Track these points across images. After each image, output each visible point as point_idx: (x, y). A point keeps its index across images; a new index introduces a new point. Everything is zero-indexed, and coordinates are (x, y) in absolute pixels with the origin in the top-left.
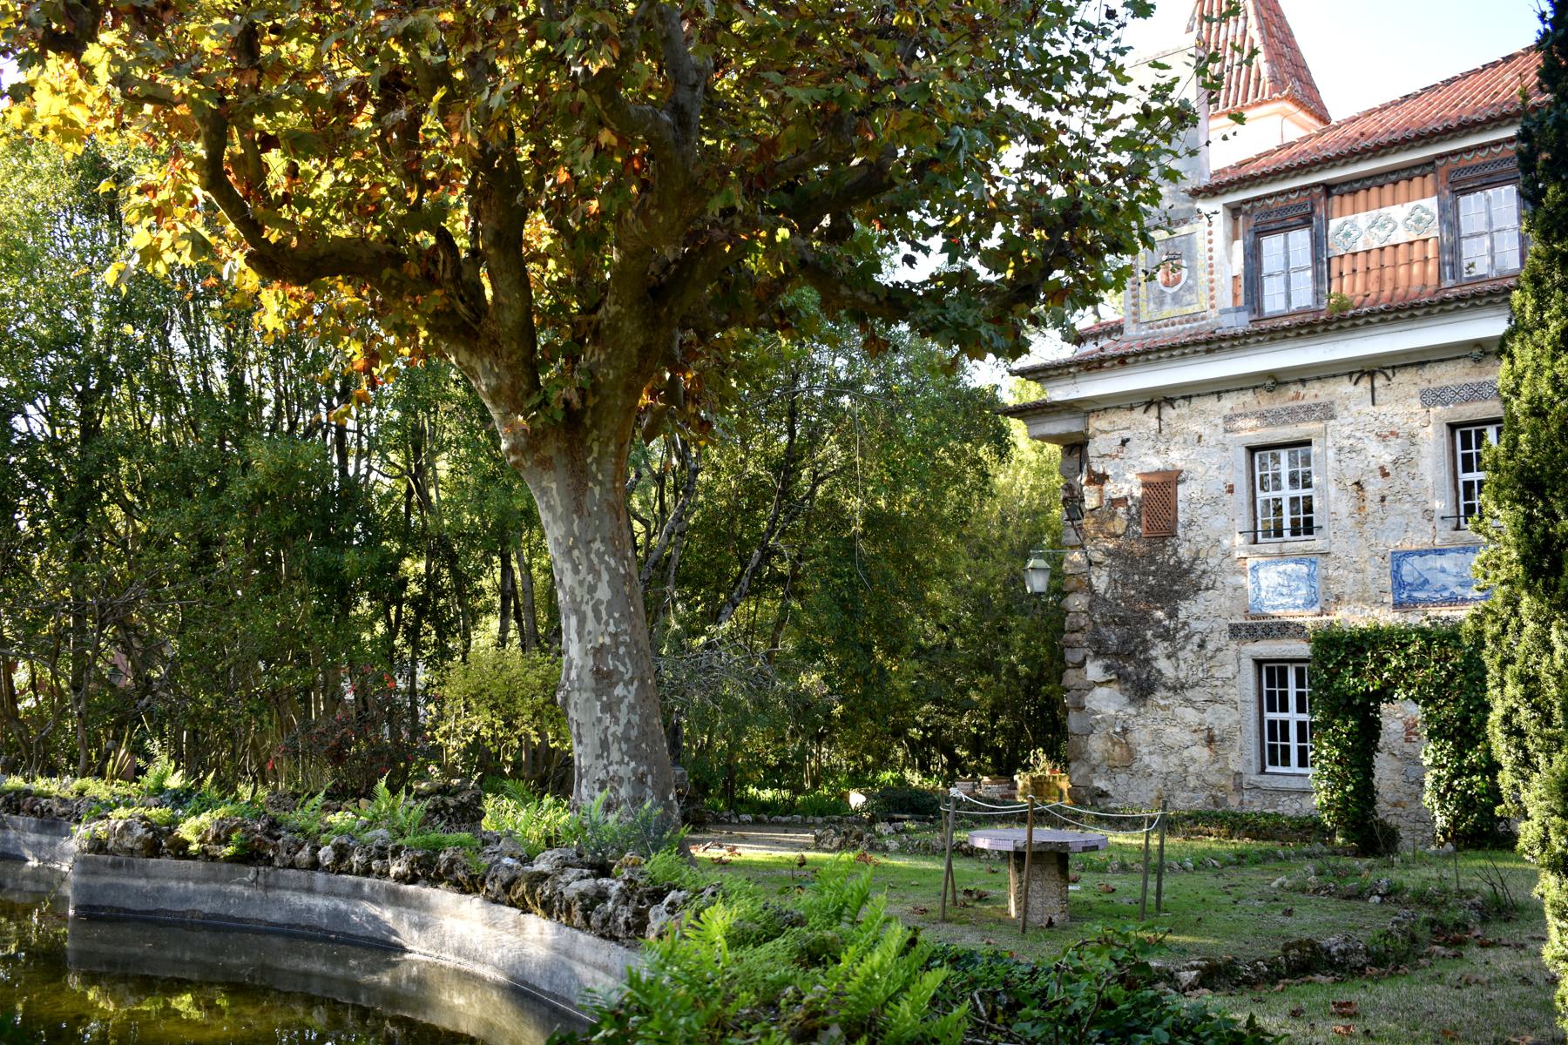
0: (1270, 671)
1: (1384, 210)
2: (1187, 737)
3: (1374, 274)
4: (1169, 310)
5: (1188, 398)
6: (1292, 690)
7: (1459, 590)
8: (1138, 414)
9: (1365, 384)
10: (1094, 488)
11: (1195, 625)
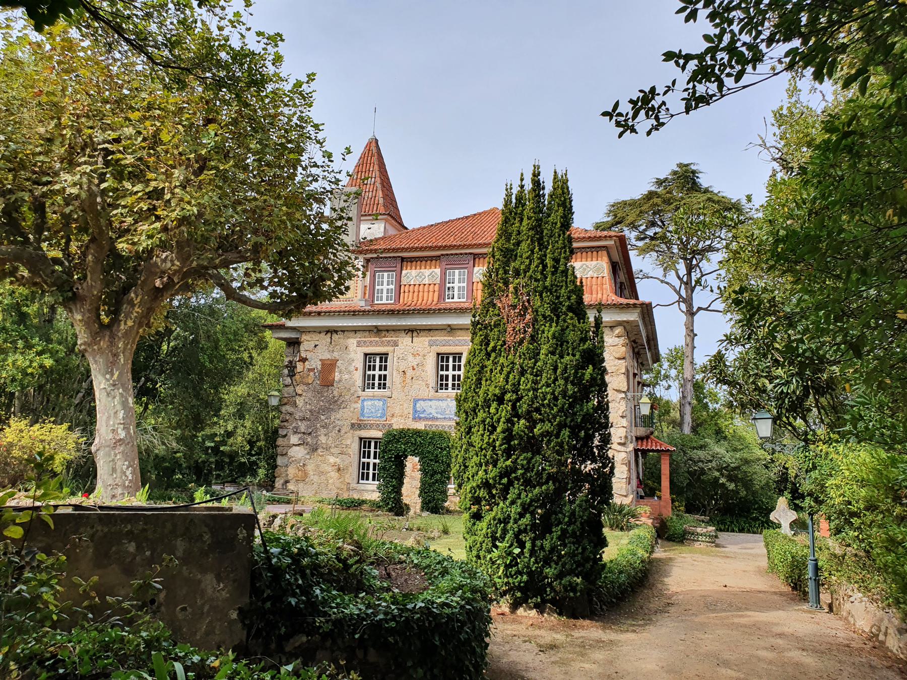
2: (330, 469)
7: (436, 415)
8: (322, 335)
10: (301, 363)
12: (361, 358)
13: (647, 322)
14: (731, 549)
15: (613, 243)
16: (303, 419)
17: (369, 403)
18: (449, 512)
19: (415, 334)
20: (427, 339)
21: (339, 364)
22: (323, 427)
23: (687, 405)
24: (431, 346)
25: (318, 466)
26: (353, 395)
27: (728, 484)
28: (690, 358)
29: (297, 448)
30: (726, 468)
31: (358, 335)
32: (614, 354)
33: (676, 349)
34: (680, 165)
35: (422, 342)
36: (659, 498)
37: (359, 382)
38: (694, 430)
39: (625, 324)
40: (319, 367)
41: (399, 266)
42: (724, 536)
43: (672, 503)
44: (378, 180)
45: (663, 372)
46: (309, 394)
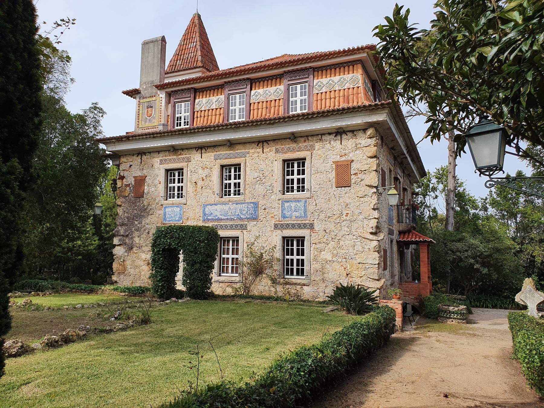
0: (288, 241)
1: (210, 98)
2: (142, 263)
3: (206, 117)
4: (147, 124)
5: (150, 153)
6: (295, 247)
7: (220, 217)
8: (135, 157)
9: (199, 151)
10: (120, 181)
11: (146, 226)
12: (162, 173)
13: (401, 127)
15: (365, 55)
16: (122, 225)
17: (170, 209)
18: (212, 297)
19: (203, 151)
20: (212, 154)
23: (451, 210)
24: (216, 159)
26: (157, 204)
27: (481, 269)
28: (452, 173)
29: (119, 247)
30: (479, 257)
31: (161, 155)
32: (367, 153)
35: (209, 157)
38: (457, 229)
39: (376, 126)
40: (133, 183)
41: (192, 96)
42: (478, 312)
44: (198, 43)
45: (431, 186)
46: (126, 205)
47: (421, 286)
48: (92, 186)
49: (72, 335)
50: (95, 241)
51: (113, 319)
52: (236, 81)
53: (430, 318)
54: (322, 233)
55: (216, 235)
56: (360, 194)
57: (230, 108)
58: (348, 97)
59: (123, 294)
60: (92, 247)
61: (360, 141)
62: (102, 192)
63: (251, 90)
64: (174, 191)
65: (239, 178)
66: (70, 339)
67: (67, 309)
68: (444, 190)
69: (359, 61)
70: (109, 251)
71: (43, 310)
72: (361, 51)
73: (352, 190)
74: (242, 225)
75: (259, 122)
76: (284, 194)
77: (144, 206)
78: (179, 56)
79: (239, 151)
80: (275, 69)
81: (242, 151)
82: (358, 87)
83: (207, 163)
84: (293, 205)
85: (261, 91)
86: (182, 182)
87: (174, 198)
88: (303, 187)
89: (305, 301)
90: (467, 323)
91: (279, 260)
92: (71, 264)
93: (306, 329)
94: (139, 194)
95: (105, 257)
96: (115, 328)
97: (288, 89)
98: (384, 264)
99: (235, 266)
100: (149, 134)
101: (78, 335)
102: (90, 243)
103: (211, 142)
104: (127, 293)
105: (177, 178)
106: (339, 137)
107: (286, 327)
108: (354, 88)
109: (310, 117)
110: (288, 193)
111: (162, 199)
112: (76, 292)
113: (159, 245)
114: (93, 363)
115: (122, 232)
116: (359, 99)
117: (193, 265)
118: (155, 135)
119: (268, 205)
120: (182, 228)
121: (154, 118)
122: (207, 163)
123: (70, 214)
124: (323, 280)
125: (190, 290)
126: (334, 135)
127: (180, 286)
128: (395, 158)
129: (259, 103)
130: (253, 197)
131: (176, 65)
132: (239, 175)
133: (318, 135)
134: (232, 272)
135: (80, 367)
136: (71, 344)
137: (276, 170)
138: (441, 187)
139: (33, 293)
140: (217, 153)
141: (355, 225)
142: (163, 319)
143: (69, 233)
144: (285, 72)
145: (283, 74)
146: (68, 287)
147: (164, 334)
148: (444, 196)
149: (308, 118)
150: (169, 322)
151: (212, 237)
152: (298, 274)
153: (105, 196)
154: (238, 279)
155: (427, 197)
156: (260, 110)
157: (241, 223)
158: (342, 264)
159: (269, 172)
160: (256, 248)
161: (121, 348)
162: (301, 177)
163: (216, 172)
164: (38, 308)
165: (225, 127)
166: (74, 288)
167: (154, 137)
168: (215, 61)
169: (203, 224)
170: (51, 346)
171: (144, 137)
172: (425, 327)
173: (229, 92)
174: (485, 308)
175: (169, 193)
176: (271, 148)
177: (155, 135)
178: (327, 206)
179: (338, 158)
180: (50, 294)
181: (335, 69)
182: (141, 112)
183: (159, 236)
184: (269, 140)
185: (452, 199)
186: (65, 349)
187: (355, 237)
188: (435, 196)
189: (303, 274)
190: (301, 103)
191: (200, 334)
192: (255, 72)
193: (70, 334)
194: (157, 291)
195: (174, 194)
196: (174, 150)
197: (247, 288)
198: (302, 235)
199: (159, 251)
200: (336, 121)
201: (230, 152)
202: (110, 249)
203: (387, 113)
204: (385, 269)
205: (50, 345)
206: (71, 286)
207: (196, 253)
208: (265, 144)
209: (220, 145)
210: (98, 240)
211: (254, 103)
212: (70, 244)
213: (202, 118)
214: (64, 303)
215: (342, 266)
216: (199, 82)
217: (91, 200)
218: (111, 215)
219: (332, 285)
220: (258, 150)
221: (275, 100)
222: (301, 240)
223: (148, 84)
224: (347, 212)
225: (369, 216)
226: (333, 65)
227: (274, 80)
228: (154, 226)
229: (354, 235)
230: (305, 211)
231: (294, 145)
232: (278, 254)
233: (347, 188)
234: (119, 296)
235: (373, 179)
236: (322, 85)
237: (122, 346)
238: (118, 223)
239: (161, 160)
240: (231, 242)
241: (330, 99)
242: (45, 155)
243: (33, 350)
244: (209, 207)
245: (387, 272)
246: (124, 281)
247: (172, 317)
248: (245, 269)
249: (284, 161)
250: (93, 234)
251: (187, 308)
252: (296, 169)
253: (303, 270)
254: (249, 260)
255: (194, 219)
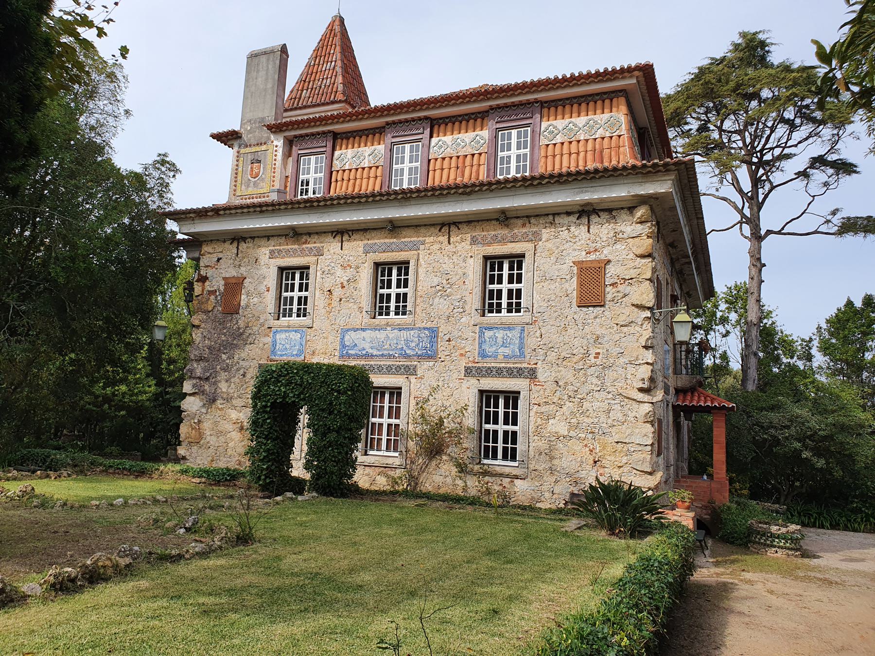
1: (360, 149)
2: (229, 427)
3: (352, 182)
4: (251, 190)
5: (253, 238)
6: (501, 410)
7: (370, 351)
8: (227, 245)
9: (338, 238)
10: (200, 284)
11: (241, 363)
12: (273, 273)
14: (829, 561)
15: (634, 81)
16: (200, 359)
17: (283, 336)
18: (356, 492)
19: (346, 237)
20: (361, 243)
21: (246, 283)
22: (225, 370)
24: (366, 252)
25: (216, 423)
26: (262, 325)
28: (756, 294)
30: (810, 437)
31: (272, 242)
33: (736, 286)
34: (743, 35)
35: (355, 248)
36: (711, 476)
37: (271, 307)
40: (222, 288)
41: (330, 145)
42: (814, 537)
43: (730, 484)
44: (339, 63)
45: (719, 314)
46: (209, 326)
47: (714, 485)
48: (153, 293)
49: (104, 567)
50: (149, 386)
51: (182, 531)
52: (407, 121)
53: (732, 543)
54: (550, 386)
55: (368, 382)
56: (622, 320)
57: (394, 166)
58: (601, 152)
59: (197, 480)
60: (144, 397)
61: (623, 228)
62: (165, 306)
63: (431, 136)
64: (291, 304)
65: (406, 286)
66: (99, 574)
67: (97, 506)
68: (738, 322)
69: (622, 92)
70: (173, 404)
71: (52, 508)
72: (626, 74)
73: (606, 313)
74: (407, 366)
75: (444, 189)
76: (484, 315)
77: (239, 328)
78: (306, 84)
79: (406, 240)
80: (475, 101)
81: (412, 239)
82: (619, 136)
83: (351, 258)
84: (500, 334)
85: (448, 139)
86: (306, 290)
87: (290, 316)
88: (518, 304)
89: (524, 508)
90: (803, 556)
91: (471, 431)
92: (108, 424)
93: (550, 569)
94: (231, 308)
95: (166, 414)
96: (188, 551)
97: (496, 137)
98: (658, 448)
99: (393, 438)
100: (254, 206)
101: (116, 566)
102: (142, 390)
103: (359, 223)
104: (203, 480)
105: (297, 282)
106: (585, 220)
107: (511, 562)
108: (611, 137)
109: (535, 183)
110: (490, 315)
111: (270, 317)
112: (114, 473)
113: (265, 396)
114: (144, 637)
115: (199, 372)
116: (621, 157)
117: (324, 435)
118: (264, 208)
119: (456, 333)
120: (307, 368)
121: (263, 180)
122: (351, 258)
123: (112, 339)
124: (552, 470)
125: (317, 479)
126: (577, 215)
127: (298, 470)
128: (672, 262)
129: (444, 159)
130: (430, 319)
131: (300, 98)
132: (406, 281)
133: (548, 215)
134: (388, 449)
135: (118, 646)
136: (100, 586)
137: (470, 273)
138: (733, 317)
139: (39, 472)
140: (369, 242)
141: (611, 375)
142: (276, 535)
143: (108, 371)
144: (492, 108)
145: (487, 112)
146: (101, 464)
147: (282, 567)
148: (738, 334)
149: (531, 185)
150: (287, 541)
151: (360, 385)
152: (505, 457)
153: (170, 312)
154: (397, 462)
155: (712, 333)
156: (445, 172)
157: (406, 363)
158: (585, 442)
159: (458, 277)
160: (432, 409)
161: (201, 600)
162: (515, 286)
163: (366, 275)
164: (45, 503)
165: (386, 197)
166: (111, 466)
167: (261, 212)
168: (365, 94)
169: (340, 363)
170: (61, 589)
171: (245, 210)
172: (733, 562)
173: (394, 140)
174: (819, 528)
175: (283, 308)
176: (463, 236)
177: (264, 208)
178: (561, 338)
179: (582, 256)
180: (69, 475)
181: (580, 104)
182: (240, 169)
183: (266, 381)
184: (460, 223)
185: (754, 337)
186: (87, 597)
187: (610, 396)
188: (724, 332)
189: (514, 458)
190: (518, 161)
191: (351, 571)
192: (440, 107)
193: (100, 564)
194: (259, 478)
195: (291, 310)
196: (295, 234)
197: (413, 479)
198: (515, 389)
199: (266, 406)
200: (582, 192)
201: (392, 241)
202: (174, 402)
203: (673, 180)
204: (659, 455)
205: (58, 586)
206: (107, 462)
207: (330, 413)
208: (453, 228)
209: (375, 229)
210: (156, 385)
211: (436, 159)
212: (109, 390)
213: (345, 182)
214: (93, 494)
215: (586, 446)
216: (343, 122)
217: (147, 316)
218: (179, 345)
219: (568, 480)
220: (441, 238)
221: (473, 155)
222: (512, 398)
223: (255, 123)
224: (598, 351)
225: (637, 359)
226: (575, 98)
227: (471, 121)
228: (255, 364)
229: (609, 393)
230: (521, 348)
231: (504, 232)
232: (471, 420)
233: (598, 309)
234: (189, 483)
235: (646, 294)
236: (556, 132)
237: (204, 594)
238: (192, 357)
239: (272, 252)
240: (387, 396)
241: (570, 154)
242: (74, 235)
243: (25, 597)
244: (352, 333)
245: (661, 460)
246: (198, 458)
247: (294, 532)
248: (411, 444)
249: (486, 258)
250: (148, 375)
251: (316, 512)
252: (506, 272)
253: (514, 450)
254: (418, 430)
255: (324, 352)
